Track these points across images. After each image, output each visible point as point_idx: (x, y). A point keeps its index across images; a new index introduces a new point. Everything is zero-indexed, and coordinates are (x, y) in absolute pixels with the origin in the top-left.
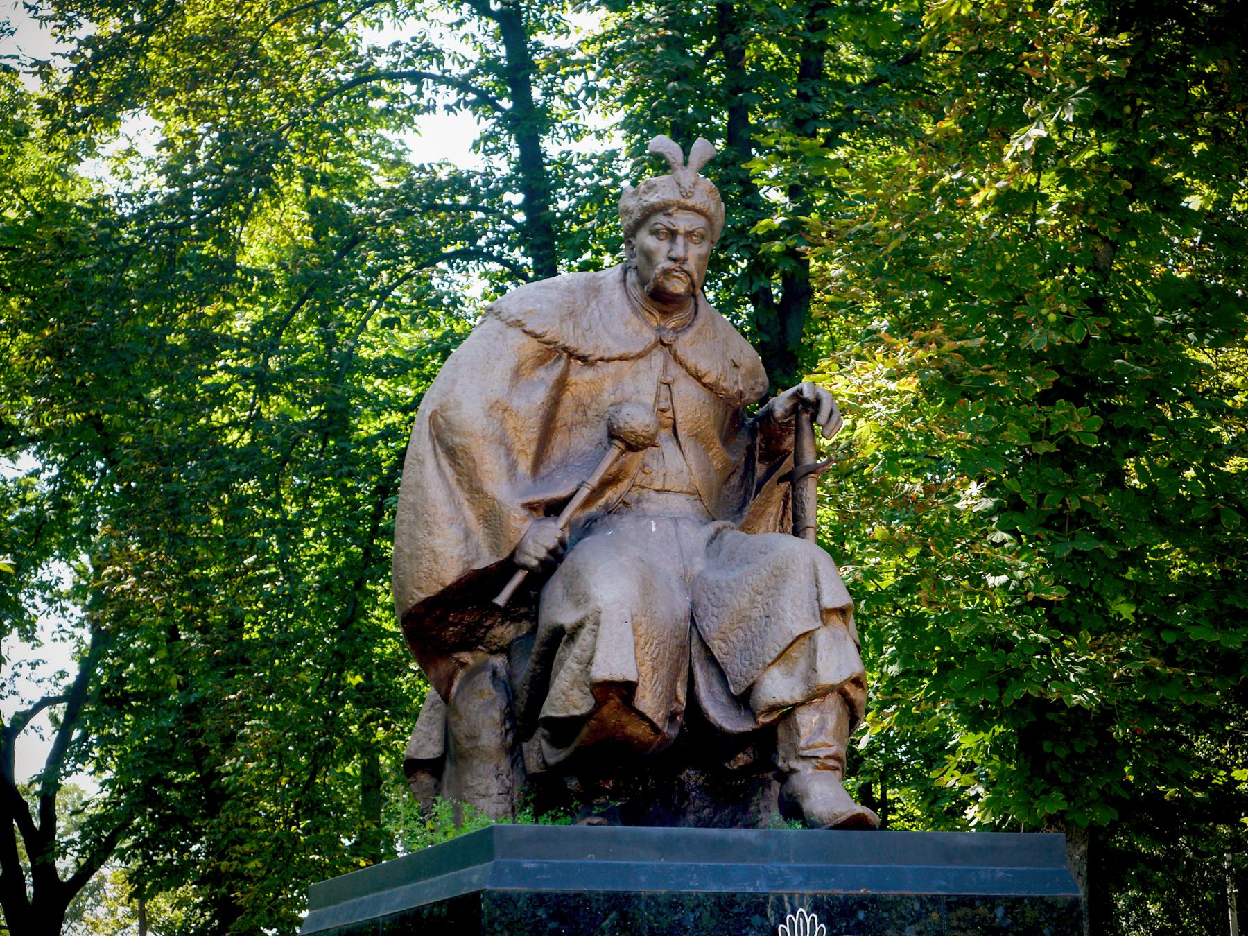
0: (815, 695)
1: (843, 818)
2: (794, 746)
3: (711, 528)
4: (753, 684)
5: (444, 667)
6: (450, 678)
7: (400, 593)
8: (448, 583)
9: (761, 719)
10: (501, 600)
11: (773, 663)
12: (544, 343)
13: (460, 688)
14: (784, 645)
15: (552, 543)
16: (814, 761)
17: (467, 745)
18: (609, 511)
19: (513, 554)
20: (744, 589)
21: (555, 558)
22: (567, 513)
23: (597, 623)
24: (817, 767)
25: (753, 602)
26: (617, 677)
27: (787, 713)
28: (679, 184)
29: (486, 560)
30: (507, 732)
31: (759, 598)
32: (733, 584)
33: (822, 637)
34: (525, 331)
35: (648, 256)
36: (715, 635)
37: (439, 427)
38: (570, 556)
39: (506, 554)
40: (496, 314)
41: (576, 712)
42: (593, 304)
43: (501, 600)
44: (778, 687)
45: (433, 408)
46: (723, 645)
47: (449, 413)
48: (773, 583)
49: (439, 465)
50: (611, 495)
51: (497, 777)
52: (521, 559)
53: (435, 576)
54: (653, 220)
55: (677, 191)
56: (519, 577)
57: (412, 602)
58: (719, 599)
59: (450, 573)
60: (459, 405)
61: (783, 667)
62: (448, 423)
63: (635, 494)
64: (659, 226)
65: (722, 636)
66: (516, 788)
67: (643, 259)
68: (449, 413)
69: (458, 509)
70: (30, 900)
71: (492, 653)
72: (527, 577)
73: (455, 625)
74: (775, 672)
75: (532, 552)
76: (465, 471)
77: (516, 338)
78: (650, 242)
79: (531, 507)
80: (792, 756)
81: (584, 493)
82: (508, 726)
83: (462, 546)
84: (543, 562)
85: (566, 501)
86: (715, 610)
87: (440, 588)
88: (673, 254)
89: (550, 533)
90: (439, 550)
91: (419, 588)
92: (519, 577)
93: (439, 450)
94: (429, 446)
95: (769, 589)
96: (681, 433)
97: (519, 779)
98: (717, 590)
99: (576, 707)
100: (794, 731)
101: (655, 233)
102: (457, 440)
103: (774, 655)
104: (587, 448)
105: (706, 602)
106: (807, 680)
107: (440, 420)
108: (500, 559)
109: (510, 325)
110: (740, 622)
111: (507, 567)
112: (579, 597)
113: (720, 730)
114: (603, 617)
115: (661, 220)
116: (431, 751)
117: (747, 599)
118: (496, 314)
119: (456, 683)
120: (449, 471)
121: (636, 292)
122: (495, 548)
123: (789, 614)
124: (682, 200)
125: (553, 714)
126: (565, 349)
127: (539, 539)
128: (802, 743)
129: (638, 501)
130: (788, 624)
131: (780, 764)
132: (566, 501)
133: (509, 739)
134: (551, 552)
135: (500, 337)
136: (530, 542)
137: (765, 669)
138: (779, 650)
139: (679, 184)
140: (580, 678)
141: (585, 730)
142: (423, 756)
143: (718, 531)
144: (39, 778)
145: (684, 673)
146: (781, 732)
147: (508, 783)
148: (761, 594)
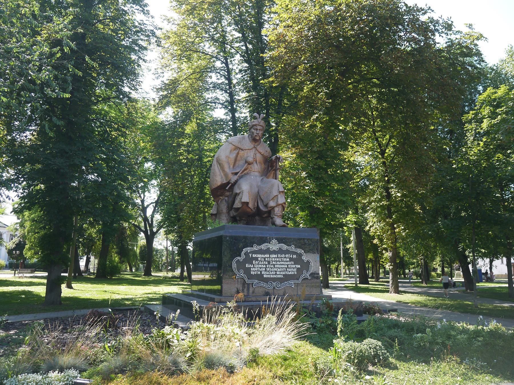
10: (227, 188)
18: (245, 174)
22: (238, 174)
29: (225, 182)
33: (279, 196)
35: (253, 133)
44: (272, 204)
50: (245, 172)
56: (230, 185)
59: (219, 184)
77: (231, 146)
78: (253, 131)
79: (232, 173)
89: (235, 178)
92: (230, 185)
111: (228, 183)
115: (255, 127)
116: (215, 212)
122: (226, 180)
127: (234, 179)
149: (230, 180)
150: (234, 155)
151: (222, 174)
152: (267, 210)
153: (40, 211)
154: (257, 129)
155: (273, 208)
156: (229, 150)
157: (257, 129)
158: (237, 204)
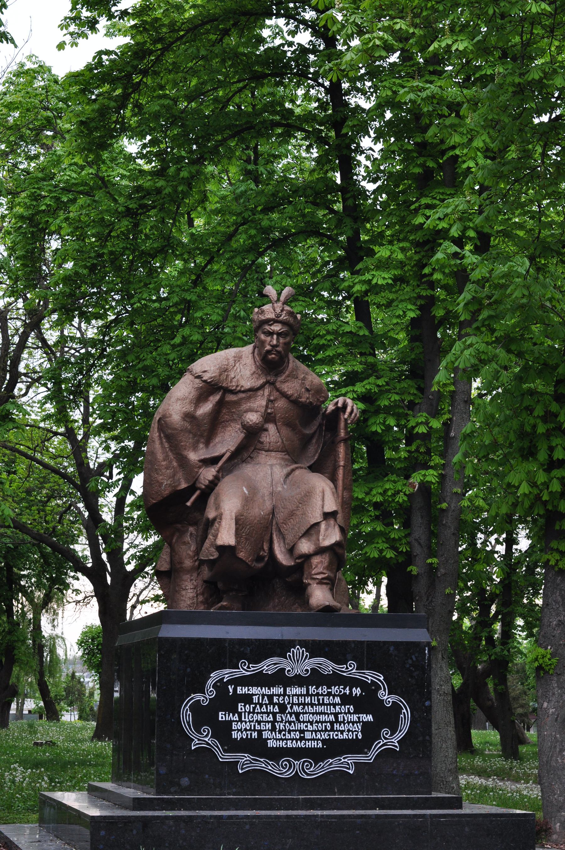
0: (320, 551)
3: (286, 471)
15: (211, 478)
17: (178, 566)
21: (214, 484)
27: (307, 557)
35: (263, 343)
38: (217, 488)
42: (237, 365)
52: (198, 485)
56: (198, 493)
70: (384, 572)
74: (303, 540)
84: (207, 486)
92: (198, 493)
101: (264, 333)
109: (196, 377)
112: (218, 507)
113: (281, 564)
120: (166, 445)
143: (293, 470)
145: (267, 537)
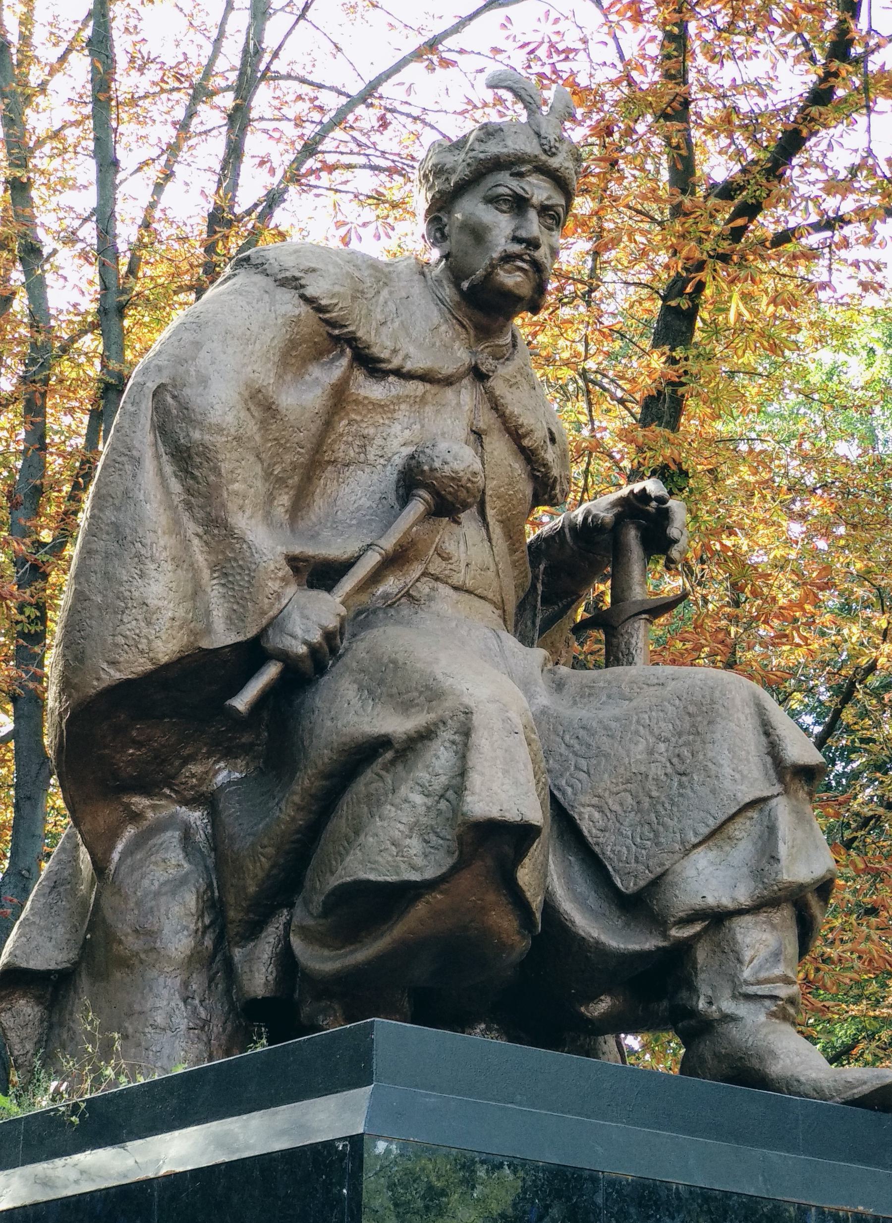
1: (866, 1089)
2: (734, 981)
4: (664, 874)
5: (105, 816)
6: (113, 835)
7: (75, 670)
8: (164, 659)
9: (674, 932)
10: (242, 702)
11: (700, 844)
12: (327, 322)
13: (124, 855)
14: (722, 817)
16: (767, 1003)
17: (132, 943)
18: (391, 604)
19: (263, 632)
20: (637, 732)
22: (348, 584)
23: (466, 732)
24: (773, 1014)
25: (651, 752)
26: (512, 816)
28: (538, 135)
29: (223, 636)
30: (206, 928)
31: (662, 747)
32: (613, 725)
33: (782, 809)
34: (303, 297)
35: (478, 234)
36: (585, 799)
37: (167, 412)
39: (252, 632)
40: (256, 266)
41: (415, 877)
43: (242, 702)
44: (709, 879)
45: (159, 381)
46: (597, 815)
47: (187, 391)
48: (687, 725)
49: (160, 471)
50: (391, 585)
51: (185, 1001)
53: (143, 646)
54: (490, 180)
55: (535, 141)
56: (271, 671)
57: (96, 686)
58: (589, 746)
59: (166, 647)
60: (204, 381)
61: (712, 855)
62: (184, 407)
63: (425, 587)
64: (502, 190)
65: (595, 801)
66: (215, 1021)
67: (467, 239)
68: (187, 391)
69: (186, 544)
71: (185, 802)
72: (283, 675)
73: (139, 745)
75: (299, 632)
76: (203, 489)
77: (288, 304)
78: (487, 215)
79: (294, 561)
80: (727, 993)
81: (372, 559)
82: (207, 921)
83: (189, 605)
85: (346, 566)
86: (583, 763)
87: (150, 667)
88: (523, 234)
89: (322, 610)
90: (153, 602)
91: (113, 663)
92: (271, 671)
93: (162, 450)
94: (150, 438)
95: (680, 735)
96: (490, 513)
97: (220, 1008)
98: (582, 733)
99: (414, 868)
100: (731, 954)
101: (493, 200)
102: (196, 435)
103: (704, 831)
104: (365, 502)
105: (563, 749)
106: (758, 874)
107: (169, 400)
108: (241, 638)
110: (628, 782)
111: (252, 654)
113: (599, 948)
114: (476, 719)
115: (506, 183)
116: (49, 956)
117: (641, 747)
118: (256, 266)
119: (120, 847)
120: (176, 486)
121: (448, 292)
122: (235, 619)
123: (727, 771)
124: (544, 157)
125: (372, 877)
126: (351, 340)
127: (311, 616)
128: (747, 973)
129: (430, 598)
130: (727, 784)
131: (702, 1005)
132: (346, 566)
133: (208, 942)
134: (329, 636)
135: (266, 296)
136: (296, 617)
137: (687, 853)
138: (713, 824)
139: (538, 135)
140: (424, 820)
141: (420, 909)
142: (36, 963)
144: (90, 15)
146: (702, 954)
147: (203, 1014)
148: (666, 740)
149: (275, 623)
150: (304, 397)
151: (201, 559)
152: (649, 943)
153: (711, 118)
154: (519, 204)
155: (717, 919)
156: (272, 338)
157: (519, 204)
158: (393, 839)
